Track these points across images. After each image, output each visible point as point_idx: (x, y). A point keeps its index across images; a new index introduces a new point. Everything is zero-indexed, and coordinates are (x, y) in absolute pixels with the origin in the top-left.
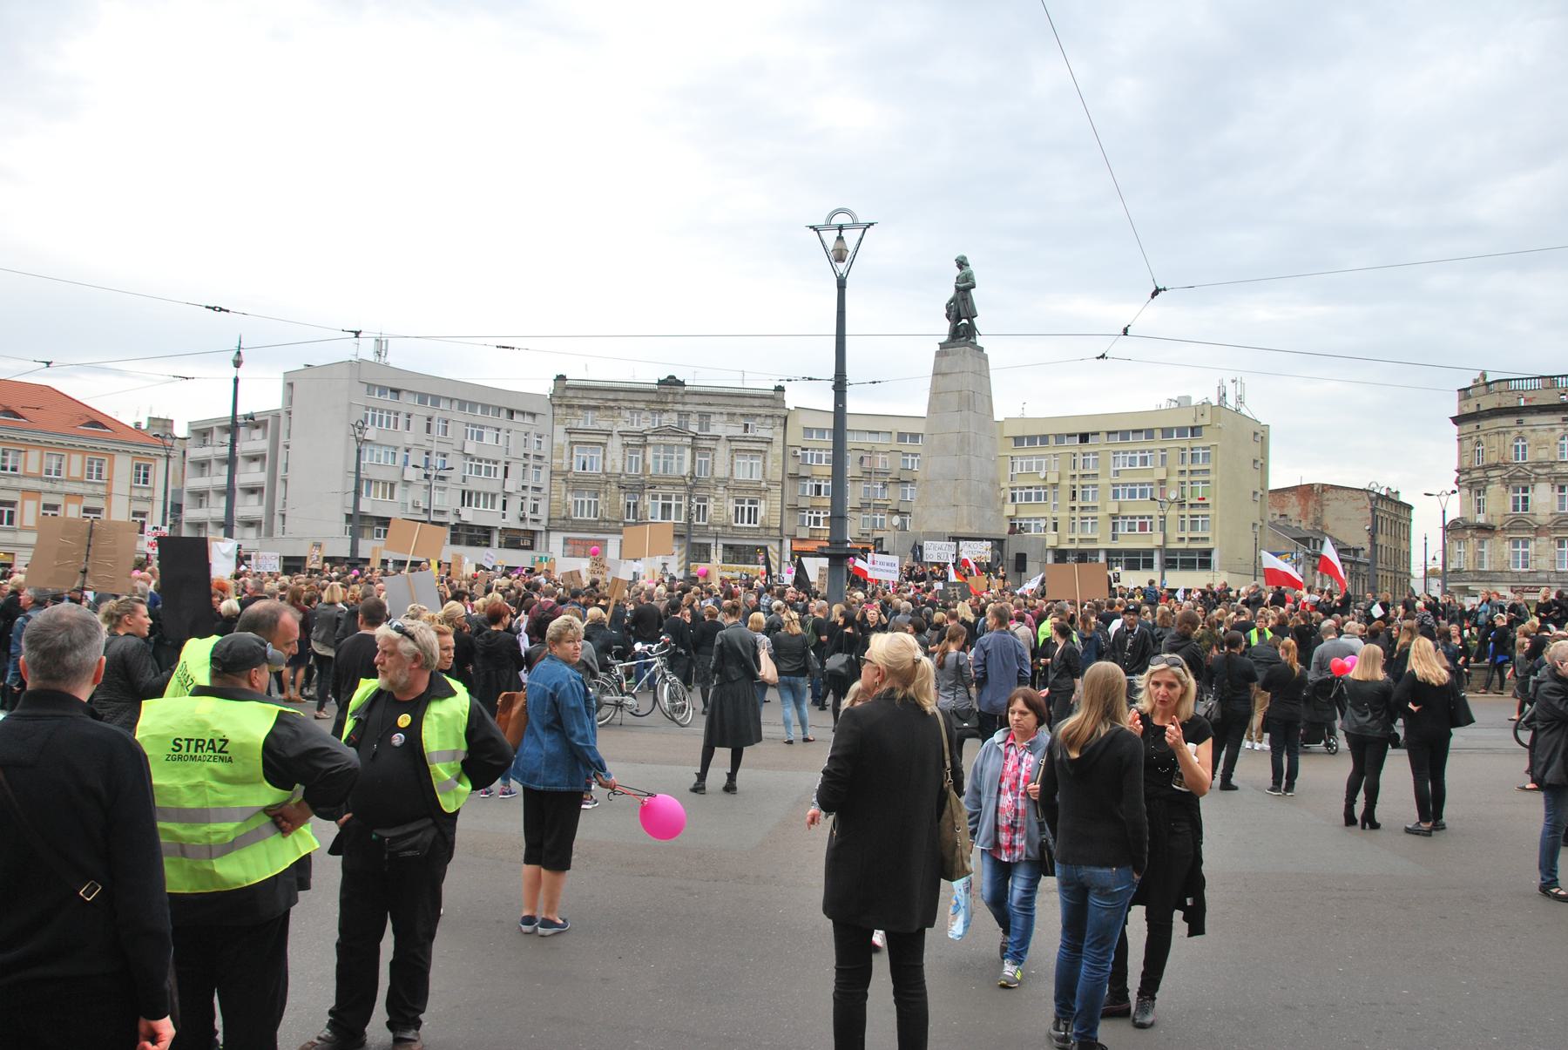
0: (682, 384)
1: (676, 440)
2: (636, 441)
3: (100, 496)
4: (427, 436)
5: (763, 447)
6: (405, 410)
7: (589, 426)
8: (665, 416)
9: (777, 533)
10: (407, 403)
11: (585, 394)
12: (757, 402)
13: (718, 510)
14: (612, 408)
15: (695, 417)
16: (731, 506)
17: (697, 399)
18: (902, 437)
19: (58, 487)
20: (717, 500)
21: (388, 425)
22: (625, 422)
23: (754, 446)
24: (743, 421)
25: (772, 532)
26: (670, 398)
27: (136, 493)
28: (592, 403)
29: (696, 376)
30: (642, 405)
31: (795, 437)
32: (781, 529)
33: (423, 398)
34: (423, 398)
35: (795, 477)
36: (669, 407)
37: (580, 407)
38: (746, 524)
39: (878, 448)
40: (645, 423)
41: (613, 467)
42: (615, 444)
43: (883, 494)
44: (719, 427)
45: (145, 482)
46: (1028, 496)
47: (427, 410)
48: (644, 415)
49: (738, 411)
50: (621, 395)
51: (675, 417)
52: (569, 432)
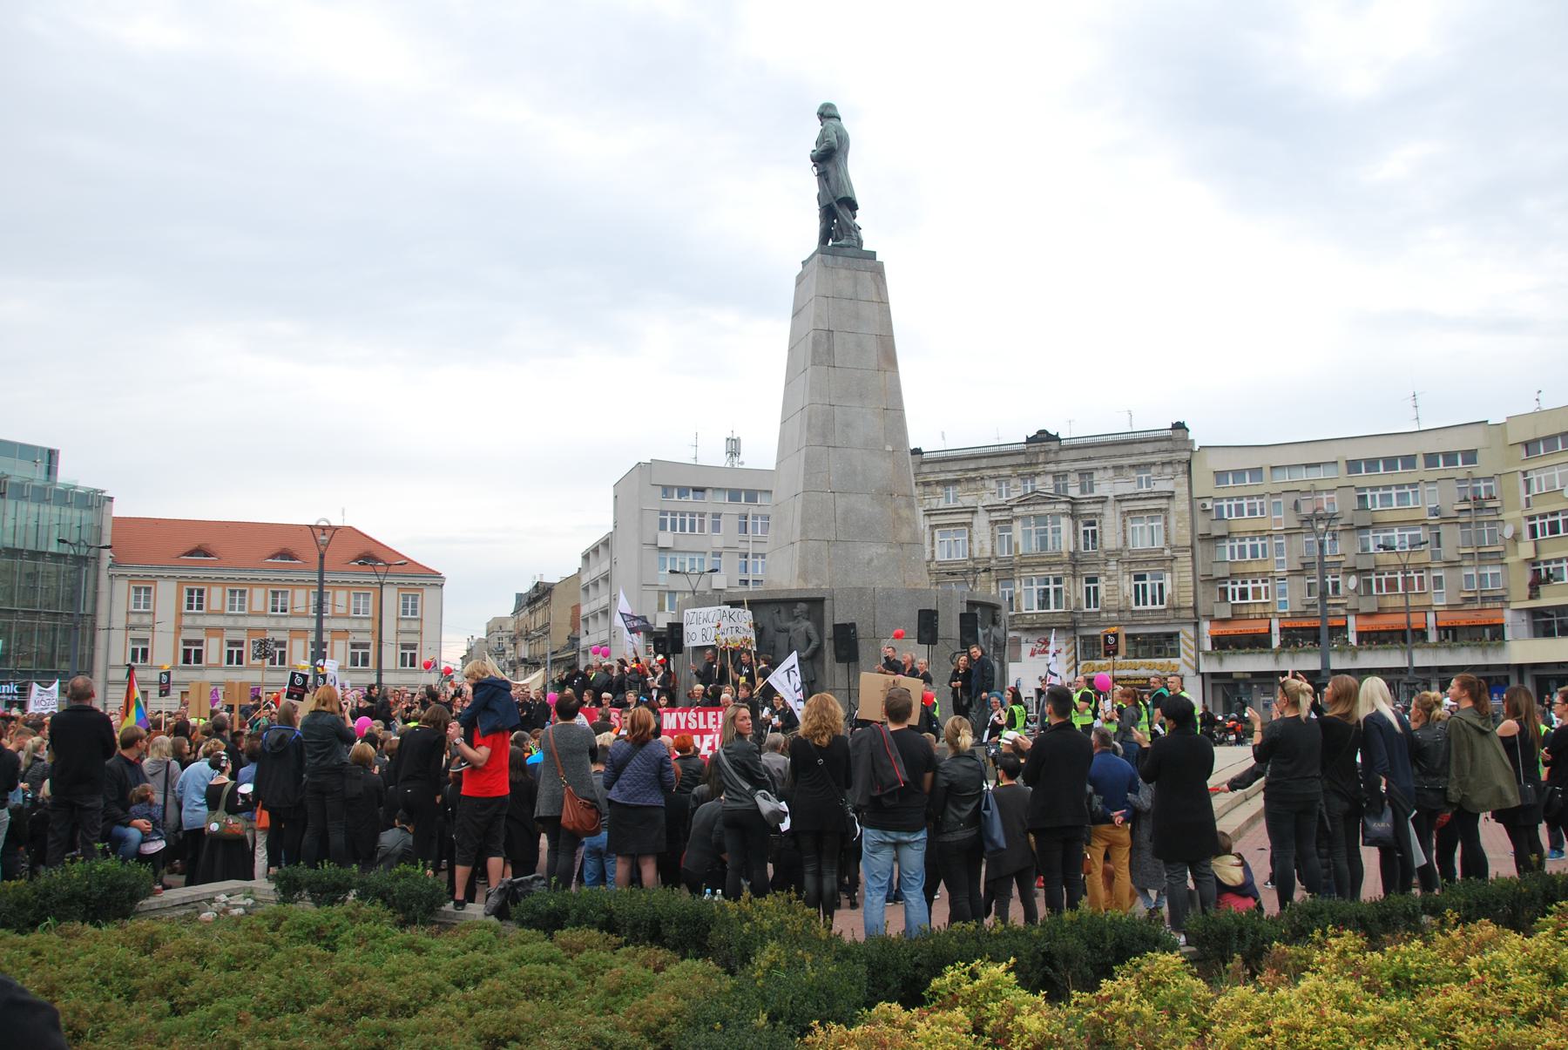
0: (1056, 438)
2: (1005, 516)
3: (415, 632)
4: (743, 536)
5: (1162, 503)
6: (710, 510)
7: (952, 504)
8: (1038, 481)
9: (1190, 614)
10: (710, 503)
11: (944, 466)
12: (1149, 448)
13: (1112, 591)
14: (973, 479)
15: (1074, 478)
16: (1128, 585)
17: (1073, 454)
18: (1353, 466)
19: (241, 622)
20: (1109, 578)
21: (692, 529)
22: (990, 494)
23: (1150, 505)
24: (1133, 474)
25: (1183, 614)
26: (1041, 458)
27: (404, 626)
28: (950, 476)
29: (1071, 425)
30: (1007, 472)
31: (1204, 485)
32: (1195, 608)
33: (734, 495)
34: (734, 495)
35: (1207, 538)
36: (1040, 468)
37: (938, 483)
38: (1149, 606)
39: (1320, 486)
40: (1017, 490)
41: (981, 550)
42: (981, 522)
43: (1333, 547)
44: (1105, 486)
45: (414, 613)
46: (1239, 509)
47: (742, 506)
48: (1013, 482)
49: (1126, 461)
50: (984, 463)
51: (1049, 480)
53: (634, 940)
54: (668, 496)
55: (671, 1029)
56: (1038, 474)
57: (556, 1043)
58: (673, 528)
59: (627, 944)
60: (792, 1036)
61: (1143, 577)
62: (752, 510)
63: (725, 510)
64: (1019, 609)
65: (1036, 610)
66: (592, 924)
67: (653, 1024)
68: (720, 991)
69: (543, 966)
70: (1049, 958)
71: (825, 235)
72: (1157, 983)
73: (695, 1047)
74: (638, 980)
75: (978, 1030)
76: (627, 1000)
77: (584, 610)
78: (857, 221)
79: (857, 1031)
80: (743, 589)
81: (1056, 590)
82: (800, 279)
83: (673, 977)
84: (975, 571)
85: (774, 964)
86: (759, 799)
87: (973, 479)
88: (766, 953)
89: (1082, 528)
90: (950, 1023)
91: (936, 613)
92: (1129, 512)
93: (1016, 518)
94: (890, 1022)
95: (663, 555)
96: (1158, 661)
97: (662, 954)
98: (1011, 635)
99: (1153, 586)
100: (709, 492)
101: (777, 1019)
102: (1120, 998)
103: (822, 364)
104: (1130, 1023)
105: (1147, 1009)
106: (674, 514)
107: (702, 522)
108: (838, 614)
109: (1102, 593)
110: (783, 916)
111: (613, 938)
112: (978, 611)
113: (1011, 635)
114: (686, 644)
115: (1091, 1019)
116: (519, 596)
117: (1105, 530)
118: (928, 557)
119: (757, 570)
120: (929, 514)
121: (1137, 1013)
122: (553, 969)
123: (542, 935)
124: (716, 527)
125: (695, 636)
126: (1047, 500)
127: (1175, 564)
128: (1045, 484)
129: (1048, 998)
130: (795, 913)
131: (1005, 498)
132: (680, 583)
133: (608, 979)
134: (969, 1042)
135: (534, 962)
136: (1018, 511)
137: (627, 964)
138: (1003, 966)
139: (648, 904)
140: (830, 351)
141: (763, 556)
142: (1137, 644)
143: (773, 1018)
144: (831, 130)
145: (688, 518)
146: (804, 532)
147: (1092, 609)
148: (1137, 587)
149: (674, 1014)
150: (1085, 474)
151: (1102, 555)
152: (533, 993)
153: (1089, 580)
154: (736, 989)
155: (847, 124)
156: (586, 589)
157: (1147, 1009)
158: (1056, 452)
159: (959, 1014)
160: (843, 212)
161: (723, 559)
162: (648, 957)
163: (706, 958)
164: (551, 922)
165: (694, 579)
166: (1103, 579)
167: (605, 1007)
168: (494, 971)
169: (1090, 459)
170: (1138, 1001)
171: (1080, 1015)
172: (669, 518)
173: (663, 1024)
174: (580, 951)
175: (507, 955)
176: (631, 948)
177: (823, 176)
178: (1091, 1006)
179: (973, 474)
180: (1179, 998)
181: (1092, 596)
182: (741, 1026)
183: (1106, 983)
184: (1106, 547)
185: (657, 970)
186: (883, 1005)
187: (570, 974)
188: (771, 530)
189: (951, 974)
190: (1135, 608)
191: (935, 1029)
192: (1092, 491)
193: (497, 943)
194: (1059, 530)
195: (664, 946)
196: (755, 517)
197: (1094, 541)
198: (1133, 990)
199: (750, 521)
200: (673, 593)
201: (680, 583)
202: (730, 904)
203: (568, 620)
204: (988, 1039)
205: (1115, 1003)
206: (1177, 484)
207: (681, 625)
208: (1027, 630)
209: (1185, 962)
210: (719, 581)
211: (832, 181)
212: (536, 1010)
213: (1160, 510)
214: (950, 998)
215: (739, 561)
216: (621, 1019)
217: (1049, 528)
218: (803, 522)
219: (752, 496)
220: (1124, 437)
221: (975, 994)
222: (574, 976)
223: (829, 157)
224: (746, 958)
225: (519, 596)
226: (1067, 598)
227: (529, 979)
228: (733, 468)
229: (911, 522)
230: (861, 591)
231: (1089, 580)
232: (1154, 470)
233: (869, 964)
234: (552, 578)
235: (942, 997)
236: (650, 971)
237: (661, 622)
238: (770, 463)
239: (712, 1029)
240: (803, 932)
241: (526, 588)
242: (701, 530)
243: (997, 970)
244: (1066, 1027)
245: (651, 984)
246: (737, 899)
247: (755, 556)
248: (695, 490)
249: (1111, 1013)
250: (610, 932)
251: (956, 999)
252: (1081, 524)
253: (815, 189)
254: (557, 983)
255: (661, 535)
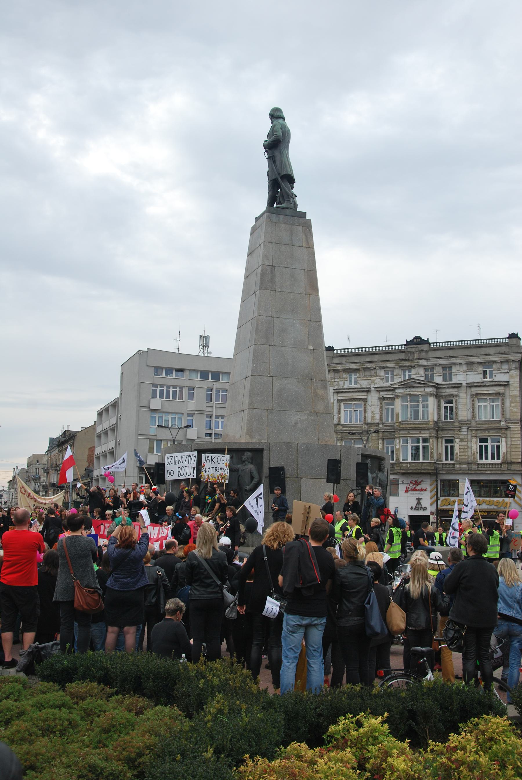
0: (427, 342)
1: (420, 391)
2: (389, 395)
4: (209, 403)
5: (501, 390)
6: (187, 384)
7: (353, 386)
8: (413, 371)
10: (188, 380)
12: (492, 351)
13: (464, 449)
14: (369, 369)
16: (475, 446)
17: (439, 354)
20: (462, 440)
21: (174, 397)
23: (492, 390)
24: (481, 369)
25: (514, 467)
26: (416, 356)
28: (353, 366)
30: (392, 364)
33: (204, 375)
34: (204, 375)
36: (415, 363)
37: (344, 371)
38: (490, 461)
41: (373, 418)
42: (373, 398)
44: (460, 377)
47: (209, 383)
49: (475, 360)
50: (376, 358)
51: (421, 371)
52: (337, 392)
53: (123, 691)
54: (156, 372)
55: (146, 759)
56: (413, 367)
57: (62, 771)
58: (161, 396)
59: (117, 693)
60: (230, 766)
61: (485, 440)
62: (216, 385)
63: (197, 385)
64: (398, 459)
65: (410, 461)
66: (93, 678)
67: (133, 755)
68: (181, 731)
69: (57, 711)
70: (412, 714)
71: (272, 200)
72: (491, 739)
73: (162, 773)
74: (124, 721)
75: (361, 766)
76: (115, 736)
77: (97, 451)
78: (294, 191)
79: (276, 763)
80: (208, 439)
81: (424, 447)
82: (254, 230)
83: (149, 719)
84: (368, 432)
85: (220, 711)
86: (379, 520)
87: (369, 369)
88: (214, 703)
89: (443, 405)
90: (342, 761)
91: (339, 462)
92: (477, 395)
93: (398, 396)
94: (299, 757)
95: (153, 414)
96: (495, 499)
97: (142, 702)
98: (391, 477)
99: (493, 446)
100: (187, 373)
101: (220, 753)
102: (464, 749)
103: (266, 289)
104: (471, 769)
105: (484, 759)
106: (162, 386)
107: (181, 393)
108: (273, 460)
109: (456, 450)
110: (228, 676)
111: (108, 690)
112: (369, 461)
113: (391, 477)
114: (167, 479)
115: (443, 764)
116: (52, 440)
117: (459, 407)
118: (336, 421)
119: (218, 427)
120: (337, 392)
121: (476, 762)
122: (64, 713)
123: (57, 687)
124: (191, 396)
125: (173, 473)
126: (419, 384)
127: (508, 432)
128: (419, 374)
129: (411, 745)
130: (236, 673)
131: (390, 382)
132: (165, 434)
133: (102, 720)
134: (355, 776)
135: (51, 707)
136: (399, 391)
137: (116, 709)
138: (380, 718)
139: (133, 664)
140: (273, 280)
141: (223, 417)
142: (481, 487)
143: (217, 752)
144: (278, 127)
145: (171, 390)
146: (251, 403)
147: (449, 461)
148: (481, 447)
149: (148, 748)
150: (447, 368)
151: (457, 424)
152: (47, 731)
153: (447, 441)
154: (193, 729)
155: (289, 122)
156: (99, 436)
157: (484, 759)
158: (427, 352)
159: (348, 753)
160: (285, 185)
161: (195, 418)
162: (131, 703)
163: (172, 705)
164: (63, 677)
165: (174, 432)
166: (457, 440)
167: (99, 742)
168: (20, 714)
169: (450, 357)
170: (476, 753)
171: (434, 760)
172: (158, 389)
173: (140, 755)
174: (84, 699)
175: (30, 702)
176: (120, 696)
177: (272, 159)
178: (442, 753)
179: (368, 366)
180: (507, 753)
181: (450, 452)
182: (195, 757)
183: (453, 736)
184: (460, 418)
185: (138, 713)
186: (295, 744)
187: (75, 716)
188: (229, 401)
189: (343, 722)
190: (480, 461)
191: (331, 764)
192: (451, 379)
193: (24, 692)
194: (427, 406)
195: (143, 695)
196: (218, 390)
197: (451, 414)
198: (473, 744)
199: (214, 393)
200: (159, 441)
201: (165, 434)
202: (191, 666)
203: (86, 457)
204: (368, 774)
205: (460, 753)
206: (511, 377)
207: (163, 465)
208: (403, 474)
209: (510, 725)
210: (192, 434)
211: (278, 163)
212: (49, 745)
213: (499, 394)
214: (342, 741)
215: (205, 419)
216: (110, 752)
217: (420, 404)
218: (250, 396)
219: (216, 376)
220: (474, 343)
221: (359, 738)
222: (78, 718)
223: (276, 144)
224: (200, 705)
225: (52, 440)
226: (432, 453)
227: (46, 720)
228: (203, 356)
229: (325, 399)
230: (288, 445)
231: (447, 441)
232: (494, 366)
233: (286, 712)
234: (76, 428)
235: (337, 740)
236: (133, 714)
237: (152, 460)
238: (229, 353)
239: (174, 760)
240: (241, 687)
241: (57, 434)
242: (181, 398)
243: (375, 722)
244: (425, 768)
245: (133, 725)
246: (196, 660)
247: (217, 417)
248: (178, 370)
249: (457, 760)
250: (106, 684)
251: (346, 741)
252: (442, 402)
253: (266, 168)
254: (66, 723)
255: (153, 401)
